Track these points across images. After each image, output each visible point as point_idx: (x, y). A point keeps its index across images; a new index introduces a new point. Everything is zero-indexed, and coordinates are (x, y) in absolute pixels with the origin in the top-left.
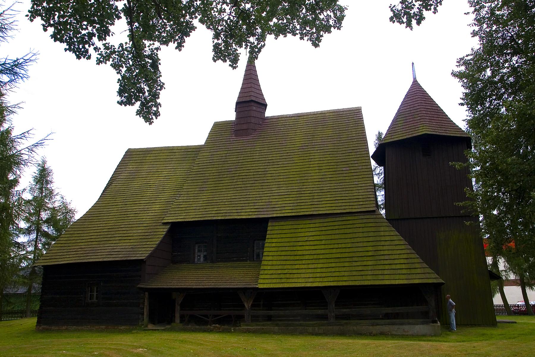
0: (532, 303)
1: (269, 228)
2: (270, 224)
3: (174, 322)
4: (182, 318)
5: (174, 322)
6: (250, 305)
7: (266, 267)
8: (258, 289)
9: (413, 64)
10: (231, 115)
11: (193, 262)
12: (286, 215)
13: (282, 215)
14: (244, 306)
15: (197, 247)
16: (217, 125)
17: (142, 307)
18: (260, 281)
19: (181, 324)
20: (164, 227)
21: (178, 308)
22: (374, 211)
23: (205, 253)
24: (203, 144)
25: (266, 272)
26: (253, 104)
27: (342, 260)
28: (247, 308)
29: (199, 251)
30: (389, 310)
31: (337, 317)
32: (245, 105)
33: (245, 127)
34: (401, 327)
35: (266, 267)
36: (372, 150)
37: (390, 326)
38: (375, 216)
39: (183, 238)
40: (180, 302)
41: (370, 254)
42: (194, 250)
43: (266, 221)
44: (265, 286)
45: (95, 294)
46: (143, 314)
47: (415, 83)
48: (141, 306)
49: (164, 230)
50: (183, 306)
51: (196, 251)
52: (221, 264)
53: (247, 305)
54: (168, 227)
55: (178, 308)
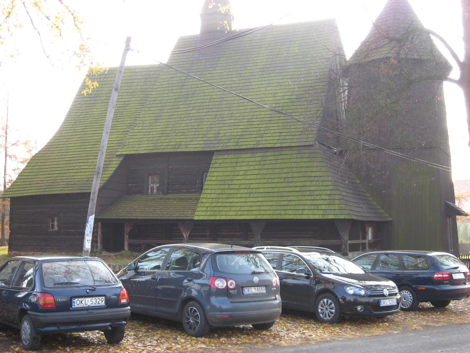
0: (469, 258)
1: (213, 162)
3: (124, 250)
4: (130, 245)
5: (124, 250)
6: (188, 236)
7: (204, 200)
11: (147, 193)
14: (183, 236)
15: (150, 178)
17: (96, 235)
19: (130, 252)
20: (117, 159)
21: (126, 237)
22: (312, 145)
23: (158, 185)
27: (271, 195)
28: (185, 238)
29: (153, 182)
35: (204, 200)
39: (132, 172)
40: (128, 231)
41: (298, 189)
42: (148, 181)
43: (211, 153)
44: (201, 218)
51: (150, 182)
54: (121, 159)
55: (126, 237)
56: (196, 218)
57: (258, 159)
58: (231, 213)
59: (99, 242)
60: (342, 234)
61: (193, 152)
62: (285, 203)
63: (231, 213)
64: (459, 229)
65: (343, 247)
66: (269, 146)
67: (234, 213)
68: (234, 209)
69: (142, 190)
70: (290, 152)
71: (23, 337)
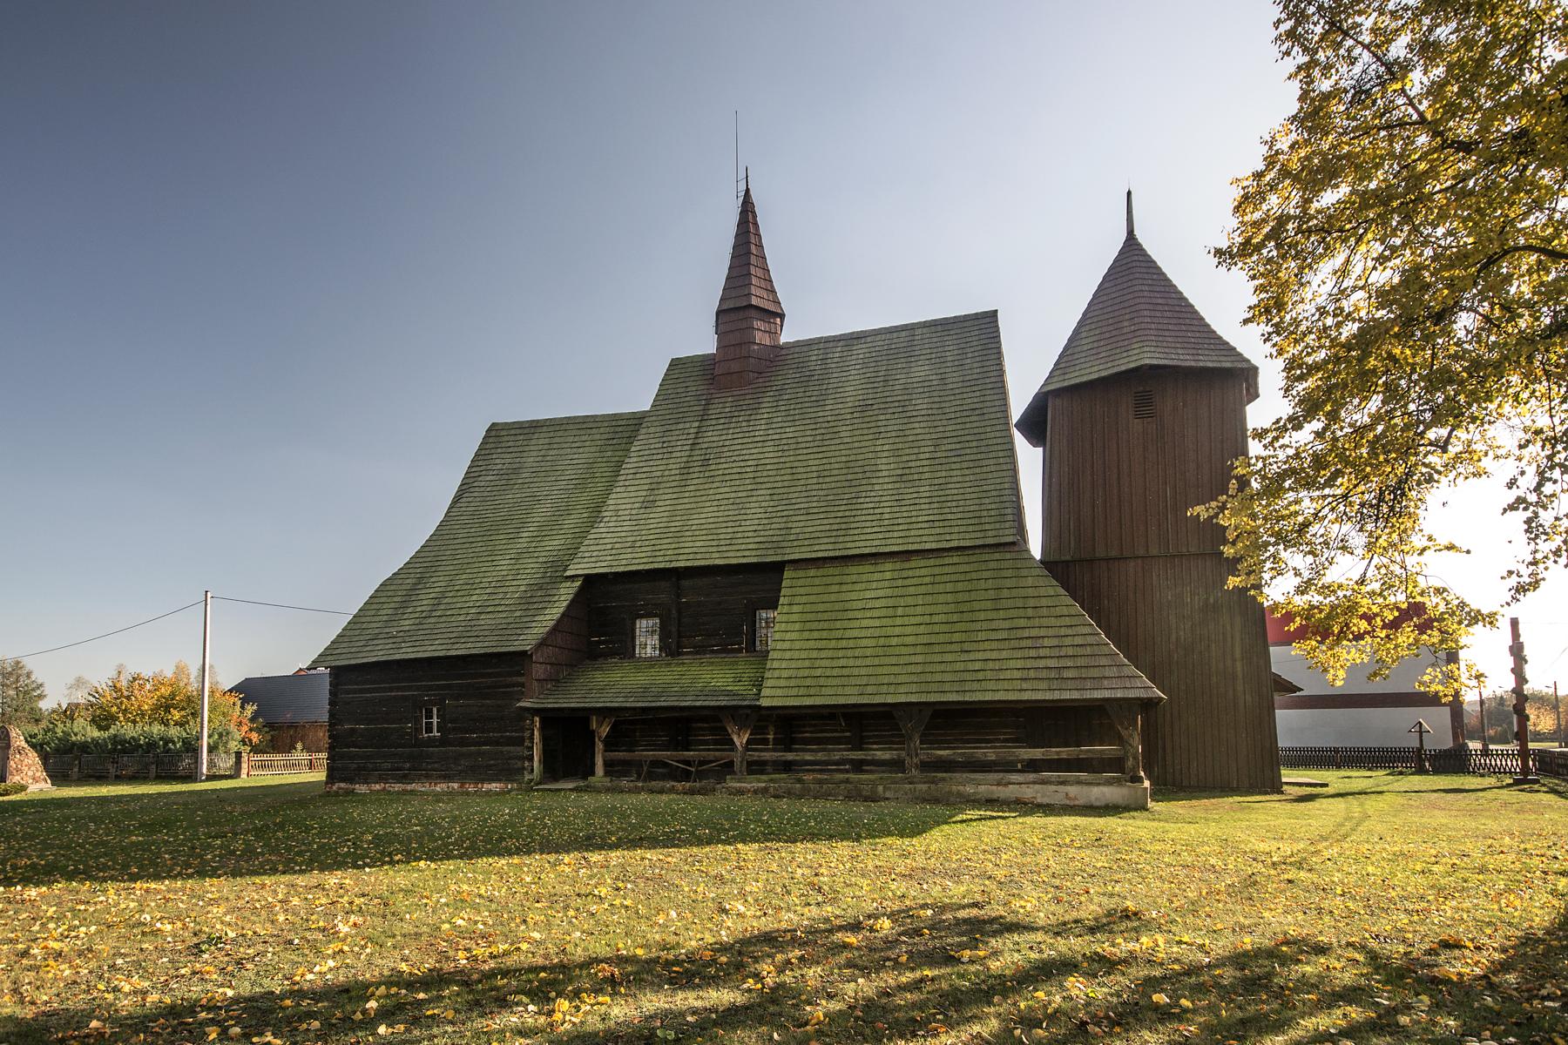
2: (786, 574)
4: (607, 764)
7: (776, 664)
8: (759, 707)
9: (1129, 193)
10: (706, 344)
12: (820, 555)
13: (814, 555)
16: (675, 363)
18: (765, 692)
21: (600, 746)
22: (1013, 543)
24: (648, 408)
25: (776, 674)
26: (753, 313)
30: (1037, 753)
31: (926, 766)
32: (733, 316)
33: (735, 366)
34: (1061, 788)
35: (776, 664)
36: (1018, 406)
37: (1037, 787)
38: (1013, 555)
39: (603, 611)
43: (777, 568)
45: (435, 720)
46: (531, 759)
47: (1131, 241)
48: (527, 743)
49: (566, 593)
50: (610, 744)
52: (436, 799)
53: (740, 740)
55: (600, 746)
56: (764, 702)
57: (888, 575)
58: (848, 690)
59: (536, 758)
60: (1124, 733)
61: (686, 568)
62: (977, 666)
63: (848, 690)
64: (716, 693)
65: (1130, 763)
66: (867, 551)
67: (855, 690)
68: (853, 681)
69: (624, 648)
70: (922, 563)
71: (33, 758)
